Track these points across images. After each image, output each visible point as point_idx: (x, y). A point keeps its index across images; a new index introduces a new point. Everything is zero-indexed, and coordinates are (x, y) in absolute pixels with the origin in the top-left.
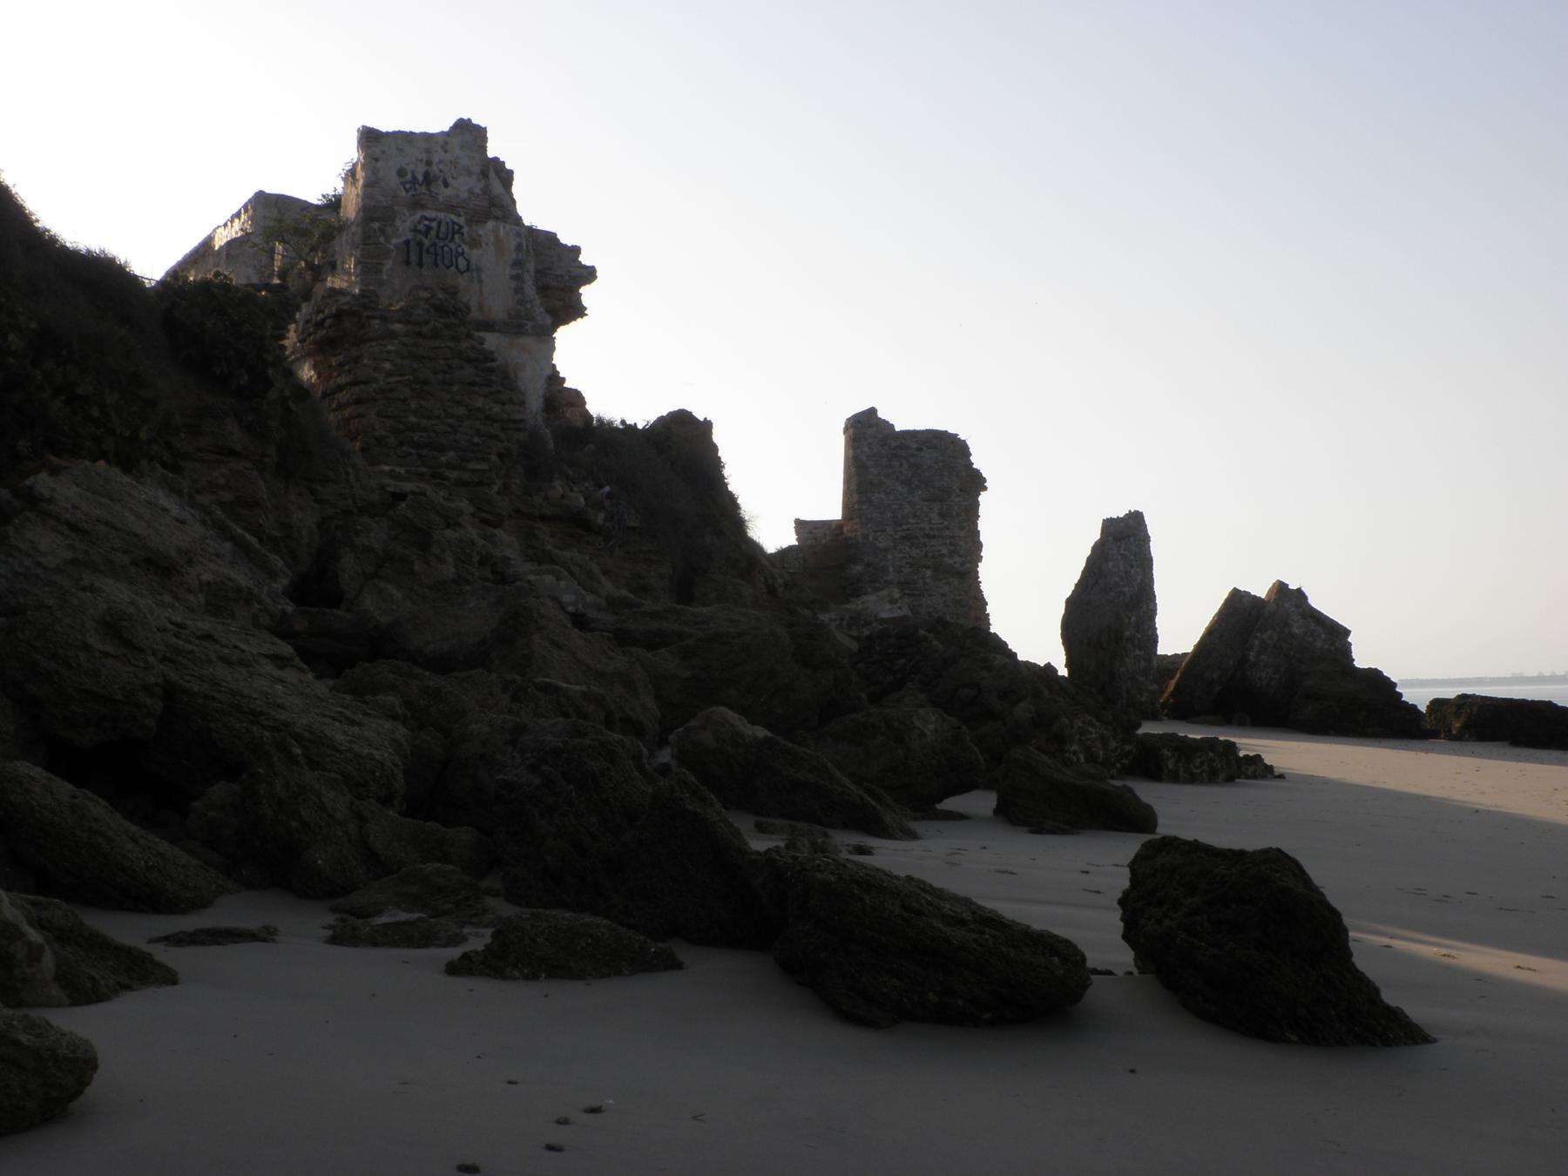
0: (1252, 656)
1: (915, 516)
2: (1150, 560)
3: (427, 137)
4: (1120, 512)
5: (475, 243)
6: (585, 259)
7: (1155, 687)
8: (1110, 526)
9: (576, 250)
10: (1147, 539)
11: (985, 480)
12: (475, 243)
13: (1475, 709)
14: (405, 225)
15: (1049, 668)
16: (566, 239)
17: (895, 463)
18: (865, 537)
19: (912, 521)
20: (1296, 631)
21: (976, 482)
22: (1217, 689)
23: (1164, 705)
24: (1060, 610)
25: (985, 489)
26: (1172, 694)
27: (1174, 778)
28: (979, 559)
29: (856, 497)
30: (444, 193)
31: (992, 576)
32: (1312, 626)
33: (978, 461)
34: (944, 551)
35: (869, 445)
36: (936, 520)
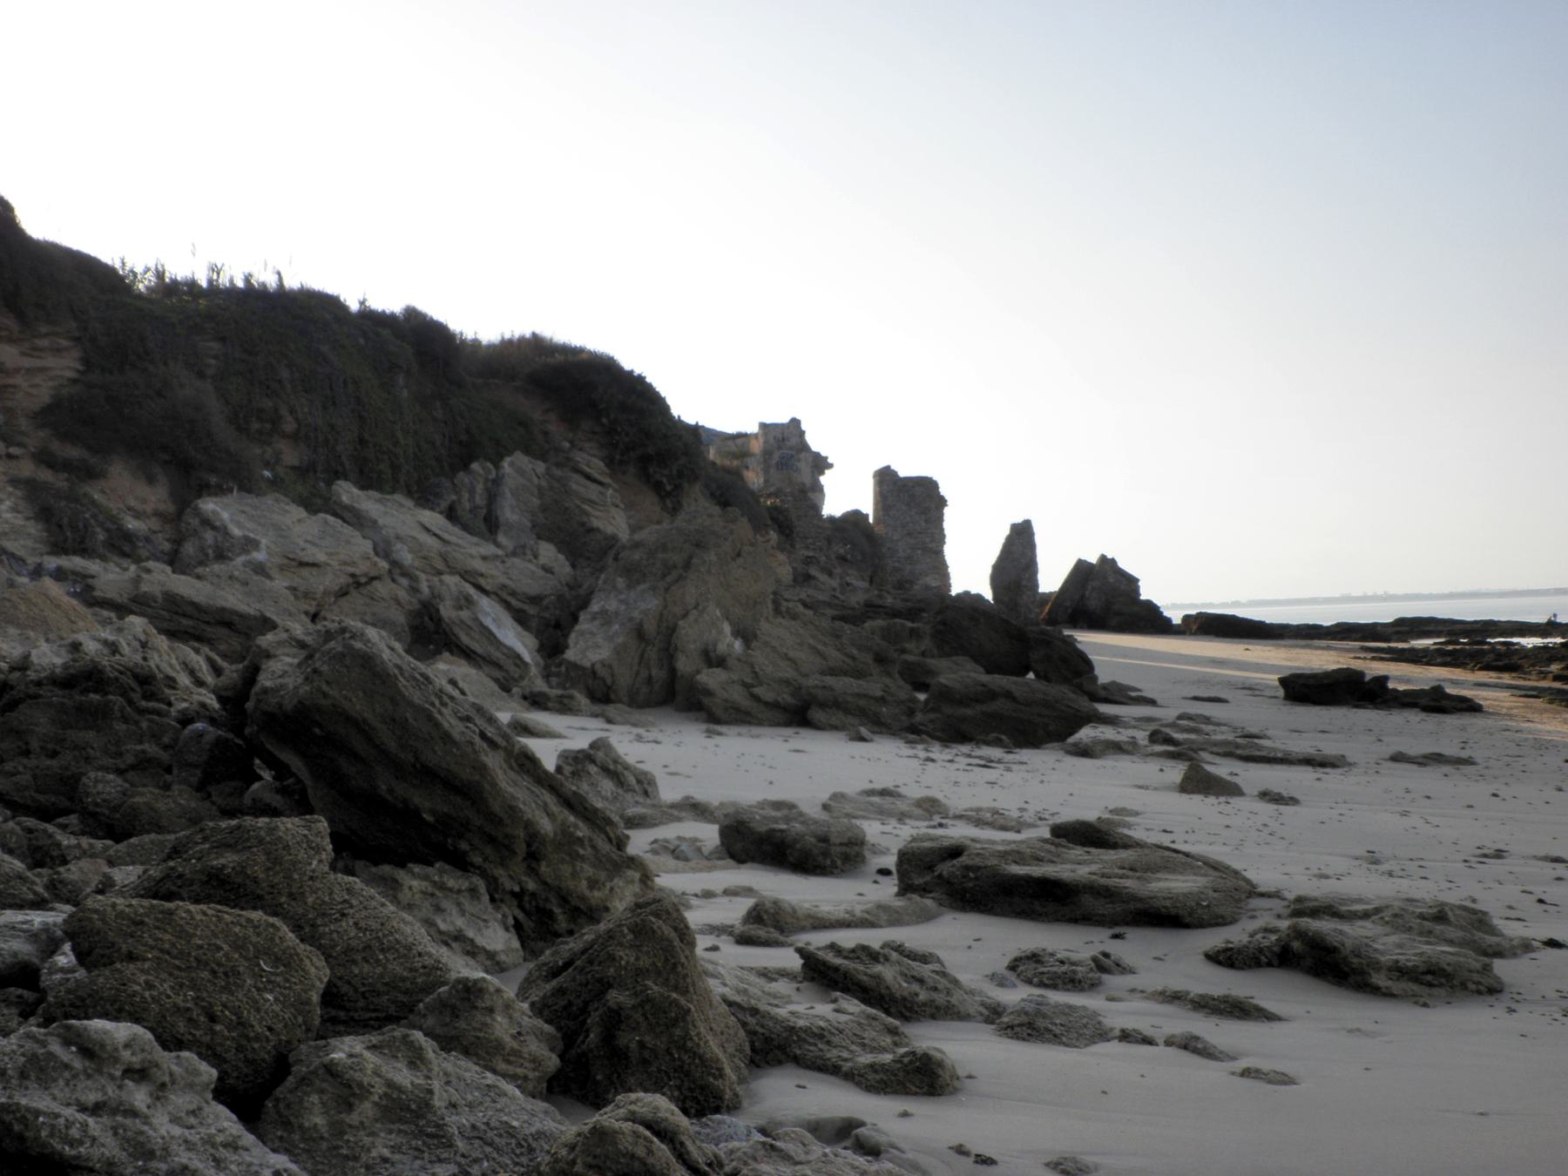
0: (1087, 593)
3: (782, 425)
4: (1019, 520)
5: (799, 460)
6: (830, 461)
7: (1038, 610)
9: (827, 458)
12: (799, 460)
14: (776, 456)
15: (979, 597)
16: (823, 454)
18: (886, 534)
20: (1111, 580)
21: (941, 502)
22: (1070, 611)
23: (1043, 619)
24: (989, 571)
26: (1048, 614)
28: (944, 543)
29: (881, 513)
30: (788, 444)
31: (951, 552)
33: (943, 491)
36: (923, 524)
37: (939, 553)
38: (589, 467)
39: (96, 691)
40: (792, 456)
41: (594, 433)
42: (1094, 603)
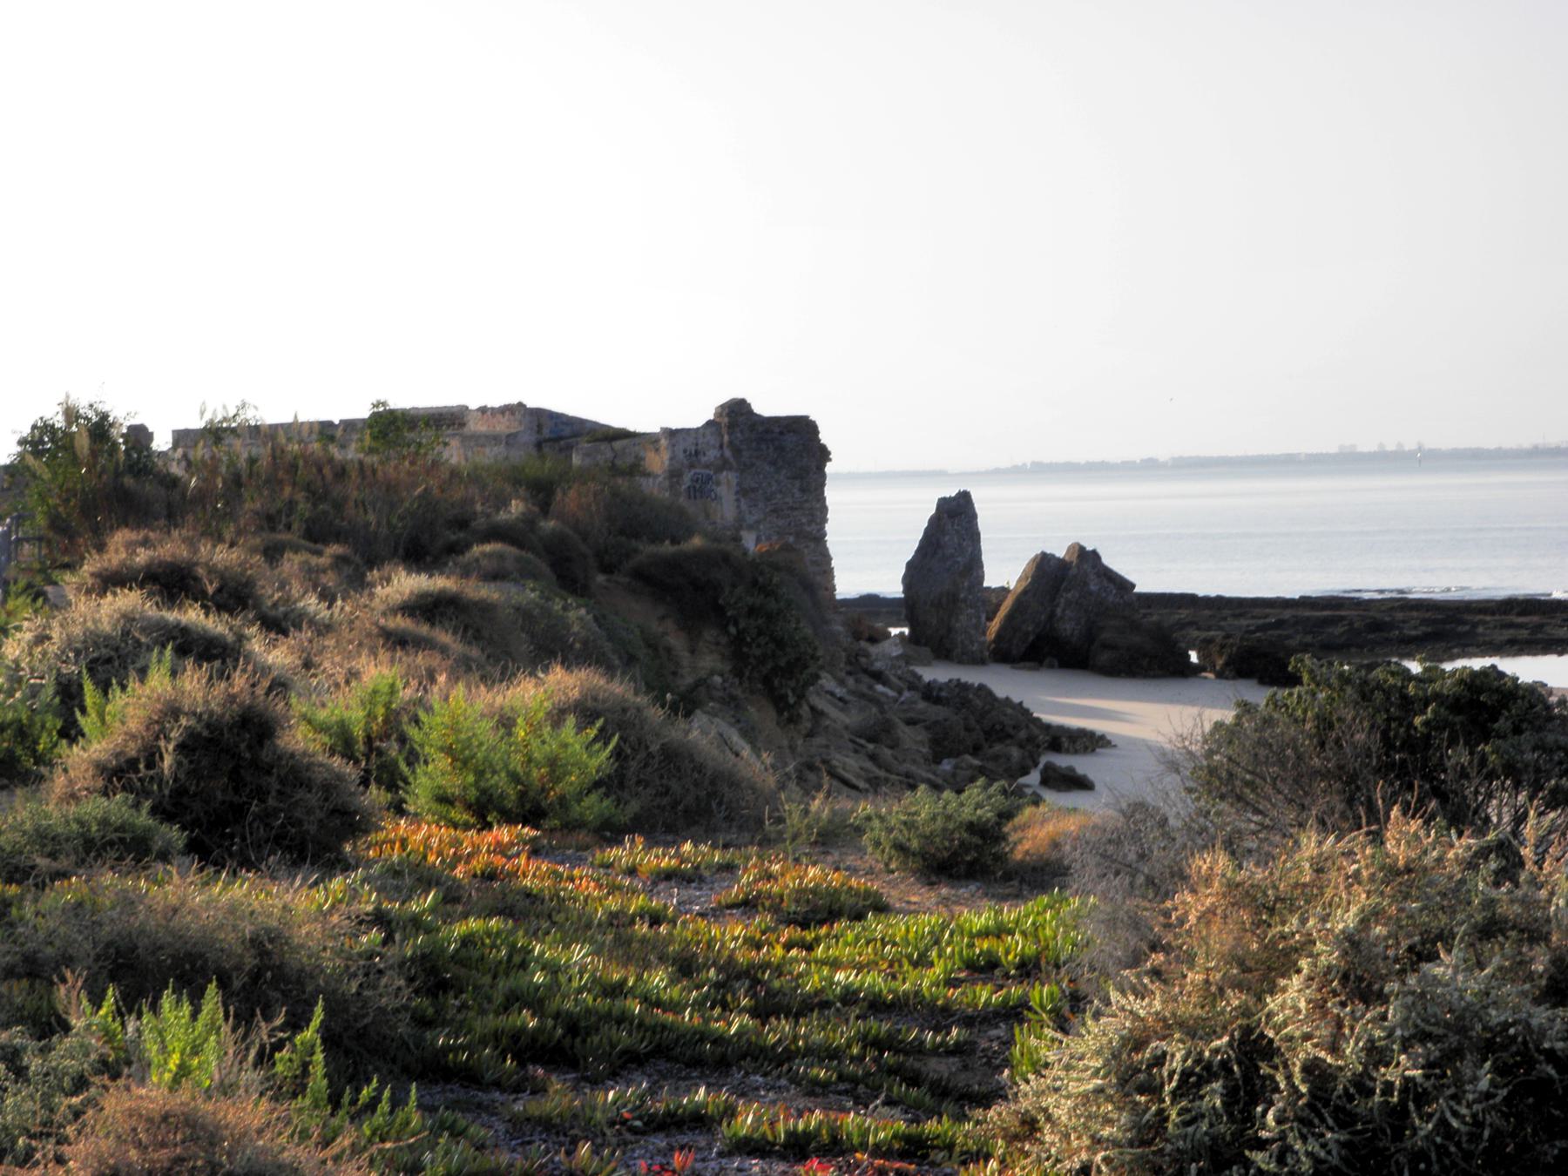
0: (1059, 611)
1: (781, 492)
2: (978, 534)
4: (951, 492)
5: (718, 484)
8: (943, 504)
10: (974, 516)
11: (829, 453)
12: (718, 484)
13: (1234, 649)
14: (687, 479)
17: (764, 447)
19: (779, 496)
20: (1093, 587)
22: (1031, 638)
25: (830, 460)
27: (1067, 751)
30: (704, 459)
32: (1105, 583)
33: (825, 437)
34: (804, 520)
35: (742, 432)
36: (798, 494)
37: (819, 538)
38: (844, 769)
39: (413, 1144)
40: (709, 478)
41: (718, 644)
42: (1069, 627)
